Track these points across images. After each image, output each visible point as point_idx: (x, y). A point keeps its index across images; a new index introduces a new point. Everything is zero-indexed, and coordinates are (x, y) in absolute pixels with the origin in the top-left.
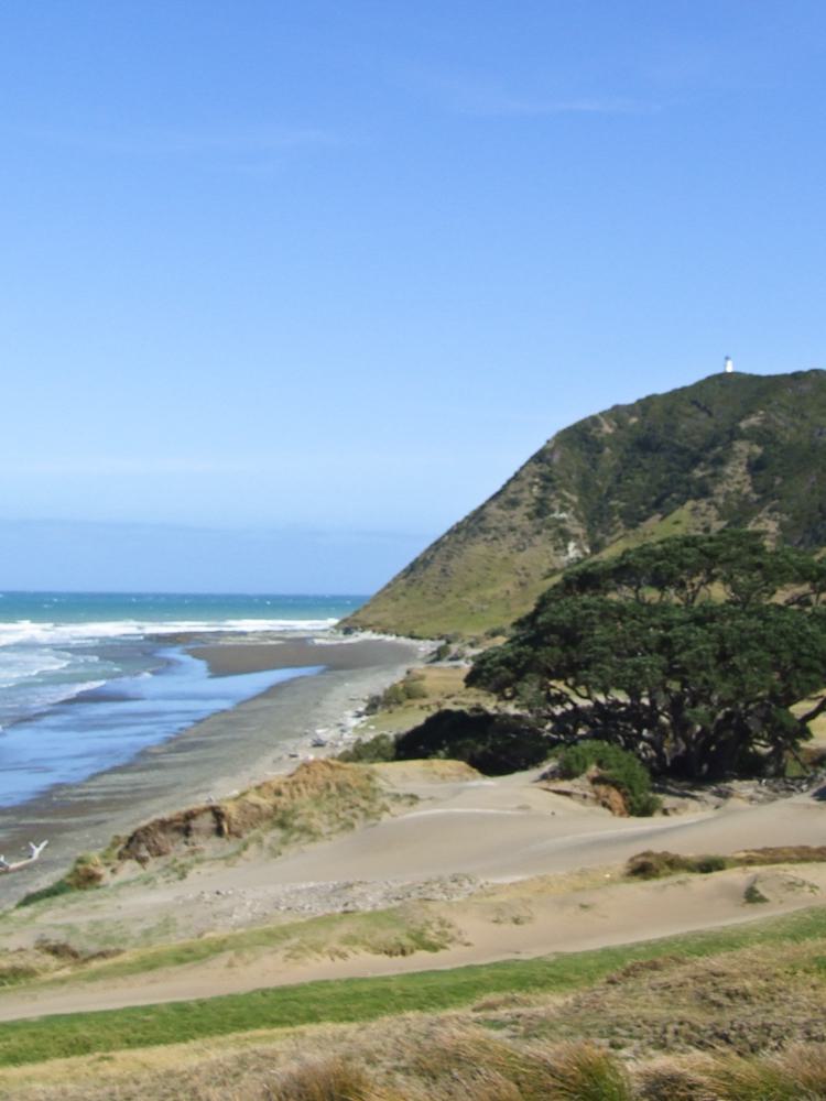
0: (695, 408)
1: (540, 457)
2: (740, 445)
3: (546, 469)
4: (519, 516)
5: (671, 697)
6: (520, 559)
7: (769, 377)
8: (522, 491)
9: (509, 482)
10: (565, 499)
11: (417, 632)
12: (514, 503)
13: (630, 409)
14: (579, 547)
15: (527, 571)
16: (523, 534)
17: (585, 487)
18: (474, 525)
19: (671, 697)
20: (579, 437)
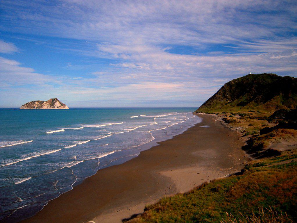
0: (212, 214)
1: (223, 87)
2: (255, 85)
3: (224, 89)
4: (221, 96)
5: (244, 169)
6: (222, 102)
7: (257, 75)
8: (221, 92)
9: (218, 91)
10: (228, 93)
11: (209, 112)
12: (220, 94)
13: (236, 80)
14: (230, 100)
15: (128, 210)
16: (222, 99)
17: (230, 91)
18: (214, 97)
19: (244, 169)
20: (229, 84)
